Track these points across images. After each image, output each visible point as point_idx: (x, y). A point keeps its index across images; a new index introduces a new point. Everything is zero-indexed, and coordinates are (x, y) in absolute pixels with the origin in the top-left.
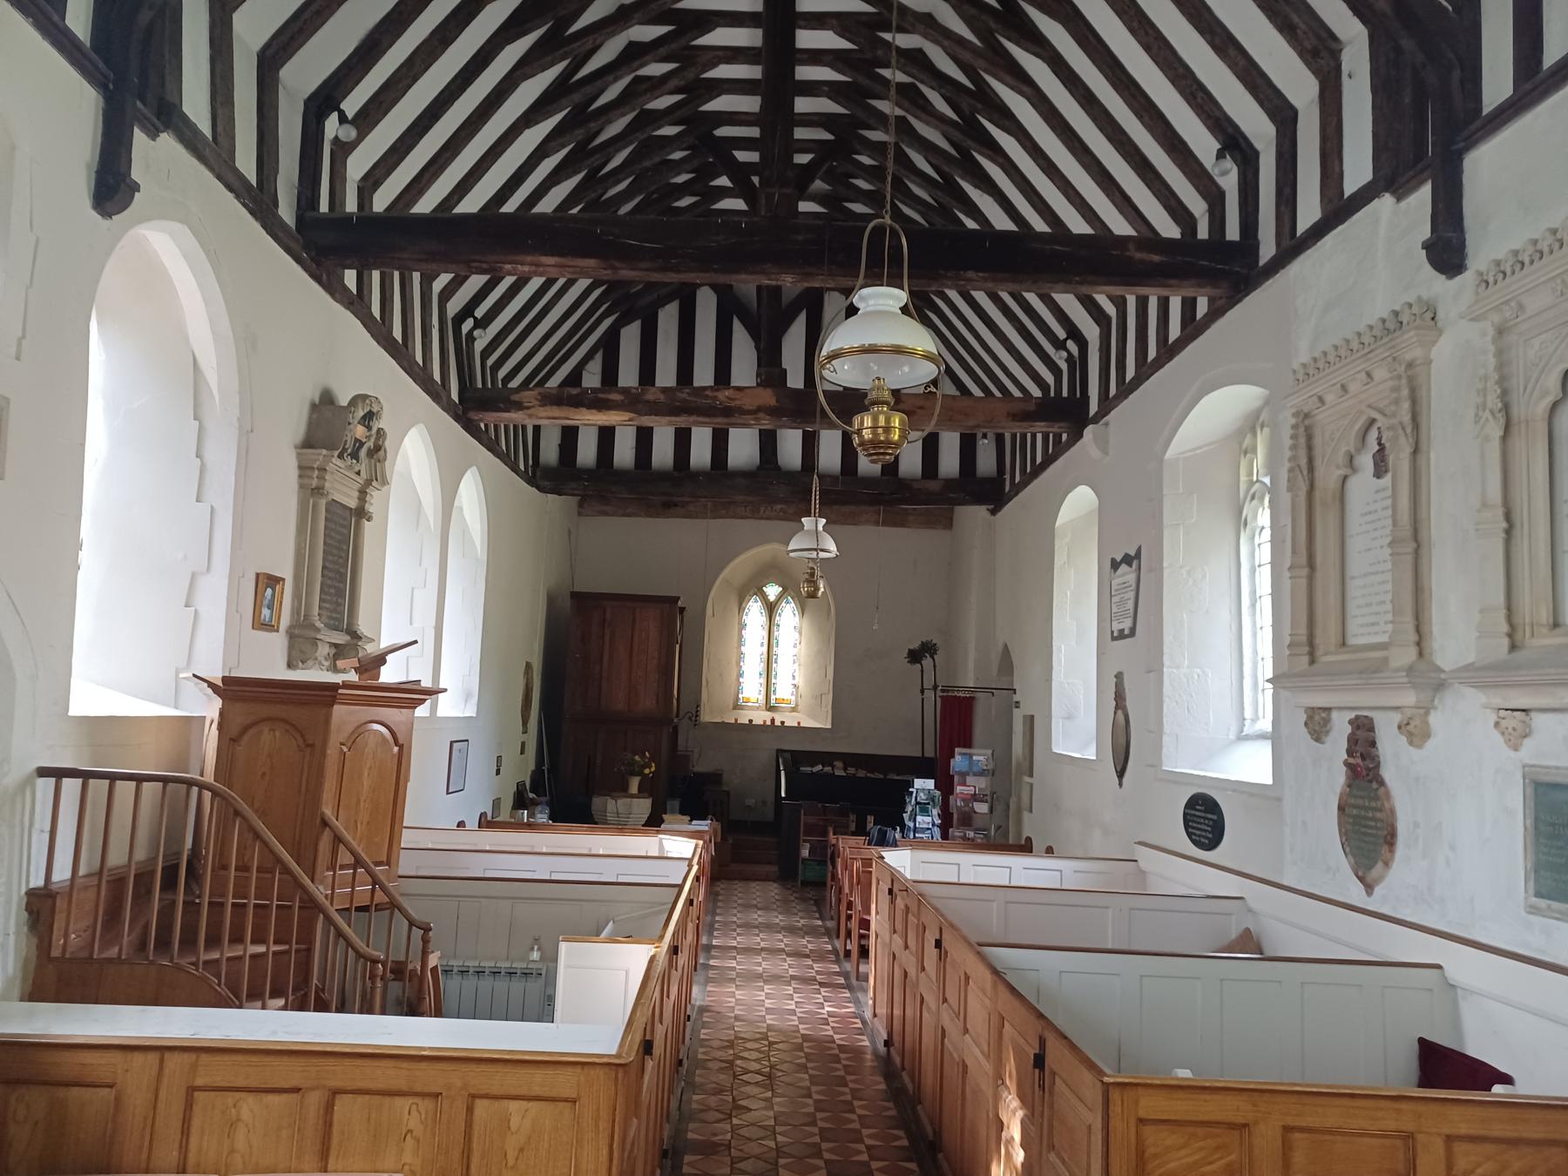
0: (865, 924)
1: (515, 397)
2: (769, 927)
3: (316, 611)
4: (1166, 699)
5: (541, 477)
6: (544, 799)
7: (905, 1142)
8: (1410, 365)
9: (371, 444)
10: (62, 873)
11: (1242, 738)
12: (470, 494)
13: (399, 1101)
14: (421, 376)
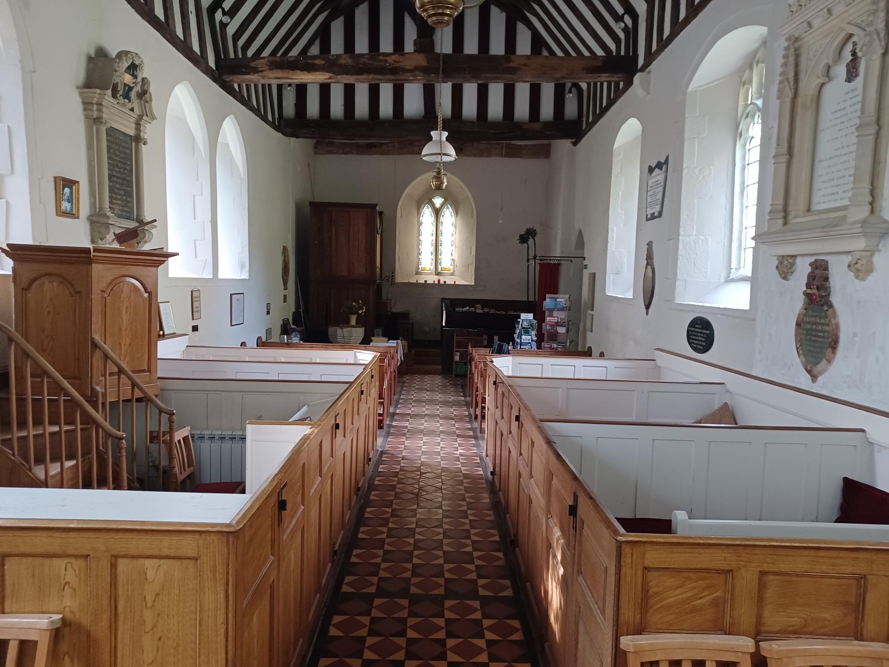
0: (484, 400)
1: (253, 64)
2: (432, 402)
3: (107, 205)
4: (680, 257)
6: (300, 329)
7: (497, 538)
9: (138, 88)
11: (729, 280)
13: (57, 562)
14: (183, 47)
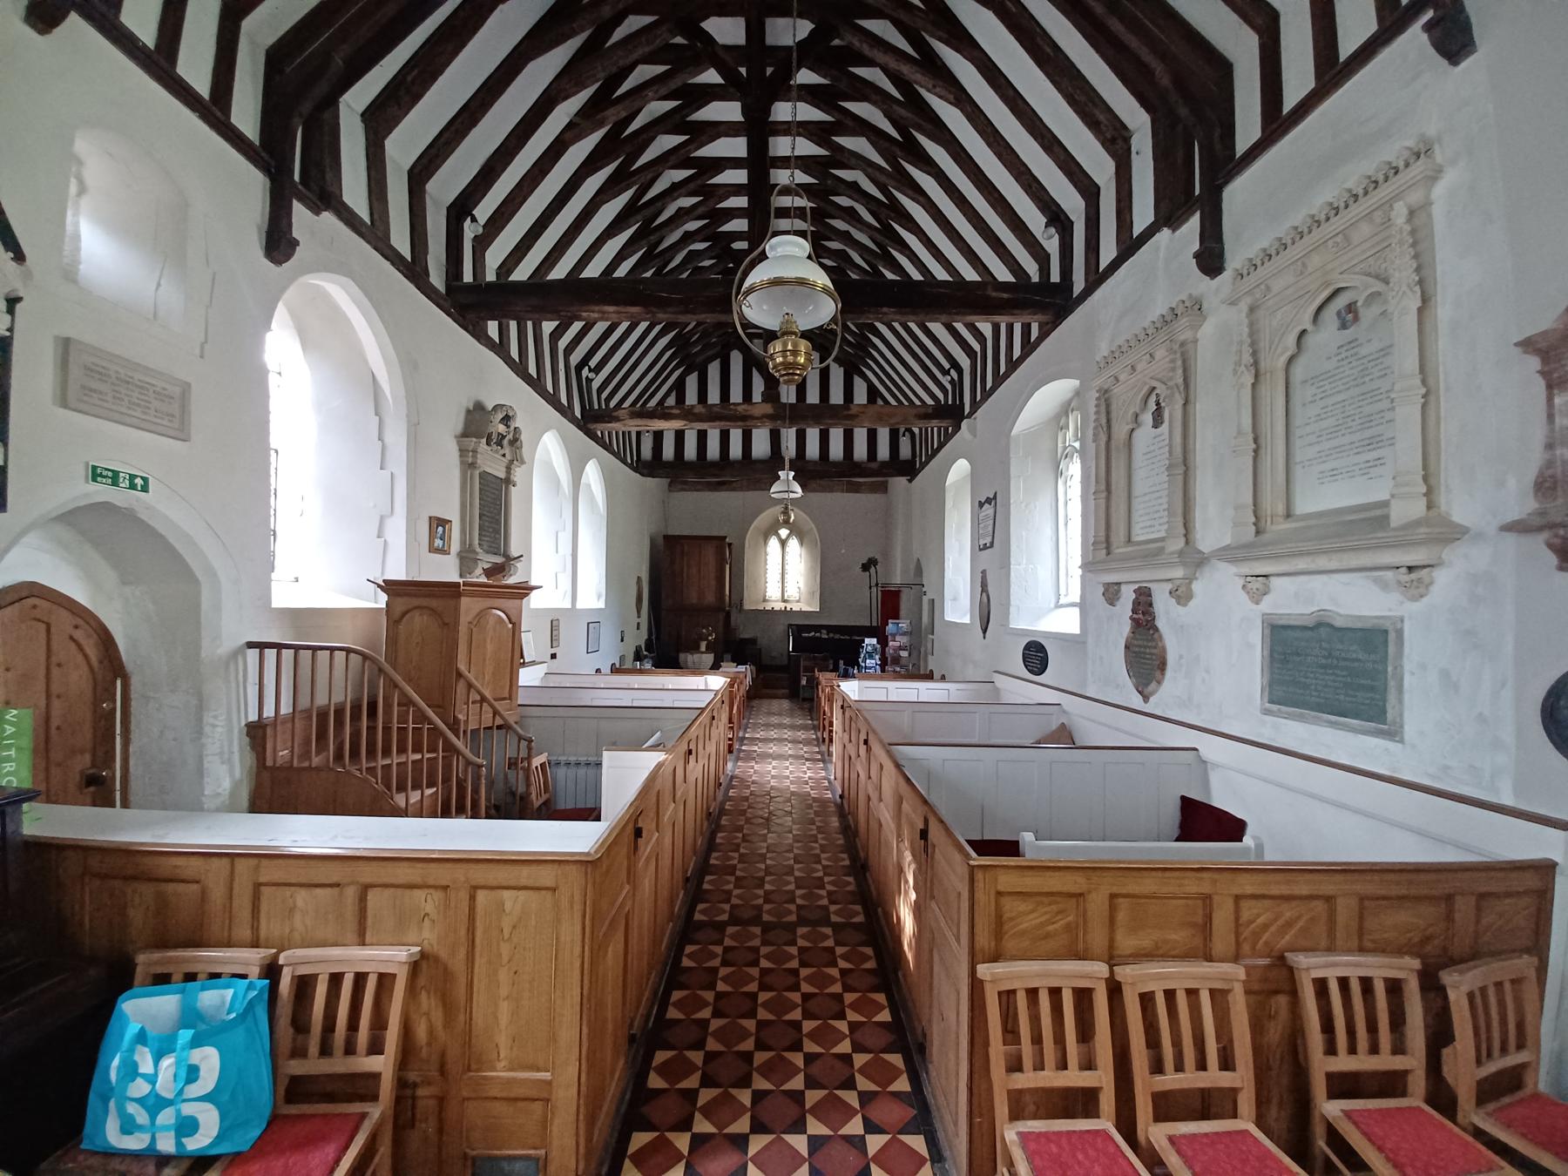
0: (831, 724)
2: (780, 726)
5: (644, 468)
8: (1182, 344)
10: (269, 712)
11: (1058, 606)
12: (592, 474)
